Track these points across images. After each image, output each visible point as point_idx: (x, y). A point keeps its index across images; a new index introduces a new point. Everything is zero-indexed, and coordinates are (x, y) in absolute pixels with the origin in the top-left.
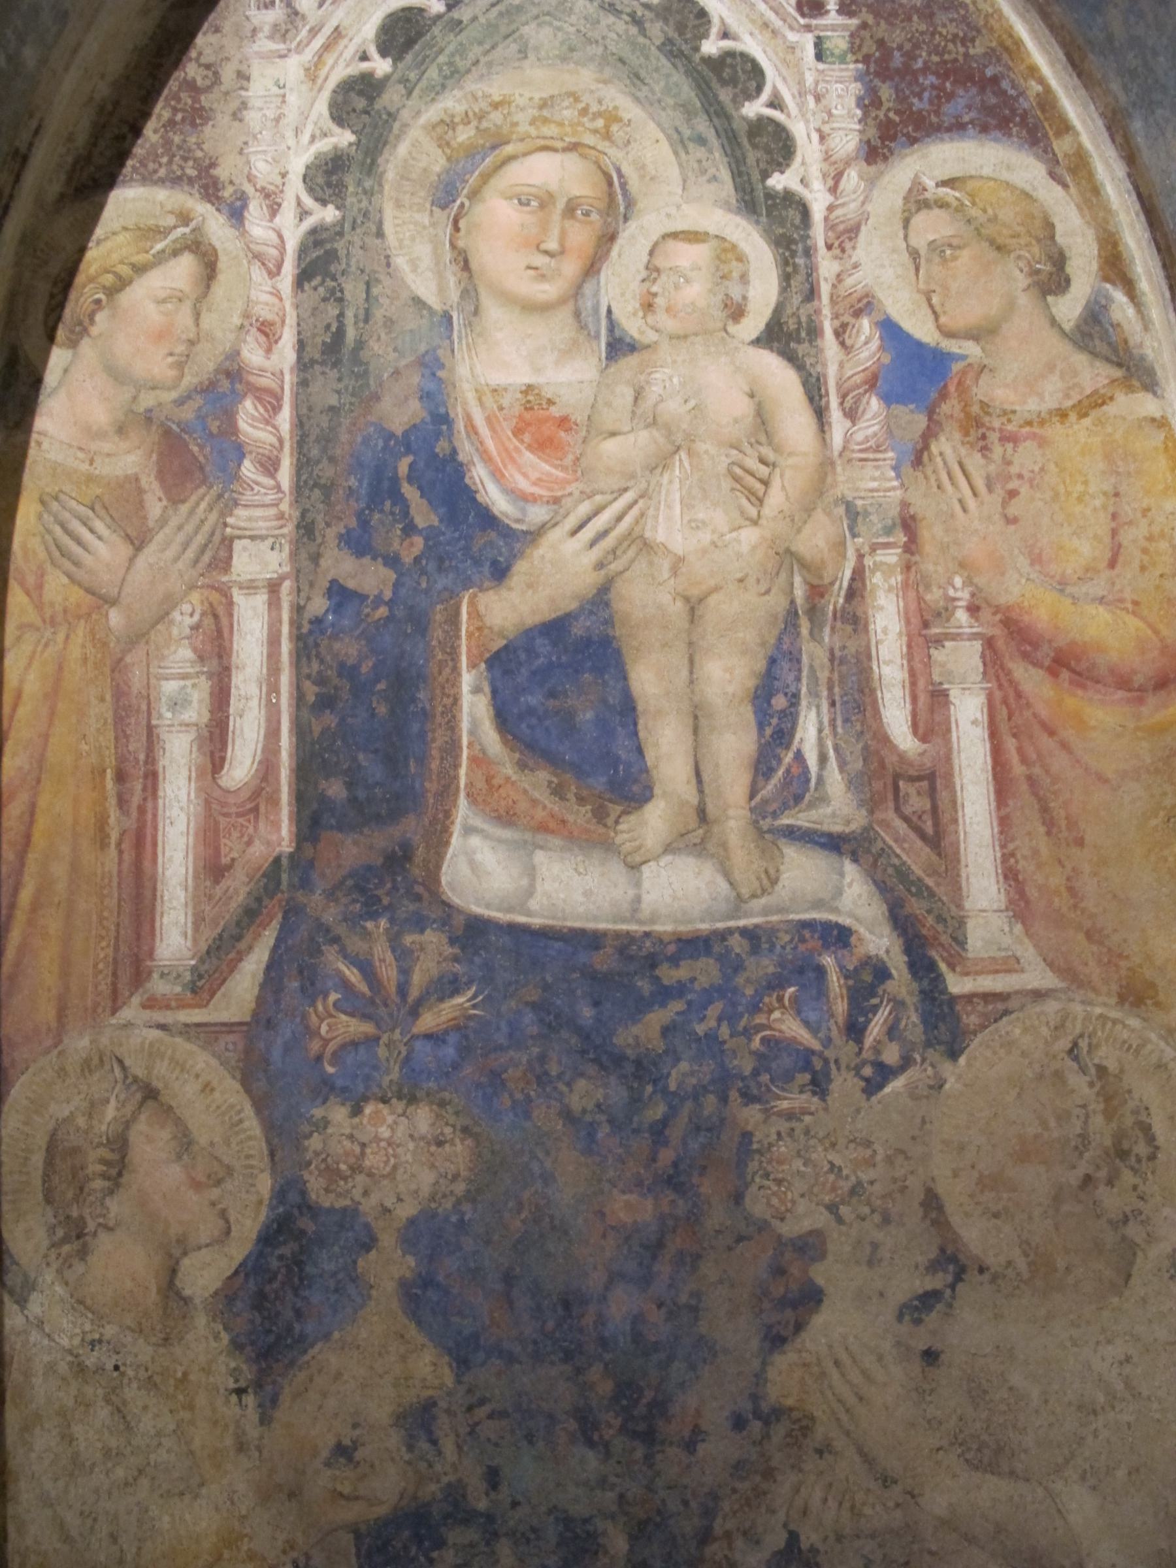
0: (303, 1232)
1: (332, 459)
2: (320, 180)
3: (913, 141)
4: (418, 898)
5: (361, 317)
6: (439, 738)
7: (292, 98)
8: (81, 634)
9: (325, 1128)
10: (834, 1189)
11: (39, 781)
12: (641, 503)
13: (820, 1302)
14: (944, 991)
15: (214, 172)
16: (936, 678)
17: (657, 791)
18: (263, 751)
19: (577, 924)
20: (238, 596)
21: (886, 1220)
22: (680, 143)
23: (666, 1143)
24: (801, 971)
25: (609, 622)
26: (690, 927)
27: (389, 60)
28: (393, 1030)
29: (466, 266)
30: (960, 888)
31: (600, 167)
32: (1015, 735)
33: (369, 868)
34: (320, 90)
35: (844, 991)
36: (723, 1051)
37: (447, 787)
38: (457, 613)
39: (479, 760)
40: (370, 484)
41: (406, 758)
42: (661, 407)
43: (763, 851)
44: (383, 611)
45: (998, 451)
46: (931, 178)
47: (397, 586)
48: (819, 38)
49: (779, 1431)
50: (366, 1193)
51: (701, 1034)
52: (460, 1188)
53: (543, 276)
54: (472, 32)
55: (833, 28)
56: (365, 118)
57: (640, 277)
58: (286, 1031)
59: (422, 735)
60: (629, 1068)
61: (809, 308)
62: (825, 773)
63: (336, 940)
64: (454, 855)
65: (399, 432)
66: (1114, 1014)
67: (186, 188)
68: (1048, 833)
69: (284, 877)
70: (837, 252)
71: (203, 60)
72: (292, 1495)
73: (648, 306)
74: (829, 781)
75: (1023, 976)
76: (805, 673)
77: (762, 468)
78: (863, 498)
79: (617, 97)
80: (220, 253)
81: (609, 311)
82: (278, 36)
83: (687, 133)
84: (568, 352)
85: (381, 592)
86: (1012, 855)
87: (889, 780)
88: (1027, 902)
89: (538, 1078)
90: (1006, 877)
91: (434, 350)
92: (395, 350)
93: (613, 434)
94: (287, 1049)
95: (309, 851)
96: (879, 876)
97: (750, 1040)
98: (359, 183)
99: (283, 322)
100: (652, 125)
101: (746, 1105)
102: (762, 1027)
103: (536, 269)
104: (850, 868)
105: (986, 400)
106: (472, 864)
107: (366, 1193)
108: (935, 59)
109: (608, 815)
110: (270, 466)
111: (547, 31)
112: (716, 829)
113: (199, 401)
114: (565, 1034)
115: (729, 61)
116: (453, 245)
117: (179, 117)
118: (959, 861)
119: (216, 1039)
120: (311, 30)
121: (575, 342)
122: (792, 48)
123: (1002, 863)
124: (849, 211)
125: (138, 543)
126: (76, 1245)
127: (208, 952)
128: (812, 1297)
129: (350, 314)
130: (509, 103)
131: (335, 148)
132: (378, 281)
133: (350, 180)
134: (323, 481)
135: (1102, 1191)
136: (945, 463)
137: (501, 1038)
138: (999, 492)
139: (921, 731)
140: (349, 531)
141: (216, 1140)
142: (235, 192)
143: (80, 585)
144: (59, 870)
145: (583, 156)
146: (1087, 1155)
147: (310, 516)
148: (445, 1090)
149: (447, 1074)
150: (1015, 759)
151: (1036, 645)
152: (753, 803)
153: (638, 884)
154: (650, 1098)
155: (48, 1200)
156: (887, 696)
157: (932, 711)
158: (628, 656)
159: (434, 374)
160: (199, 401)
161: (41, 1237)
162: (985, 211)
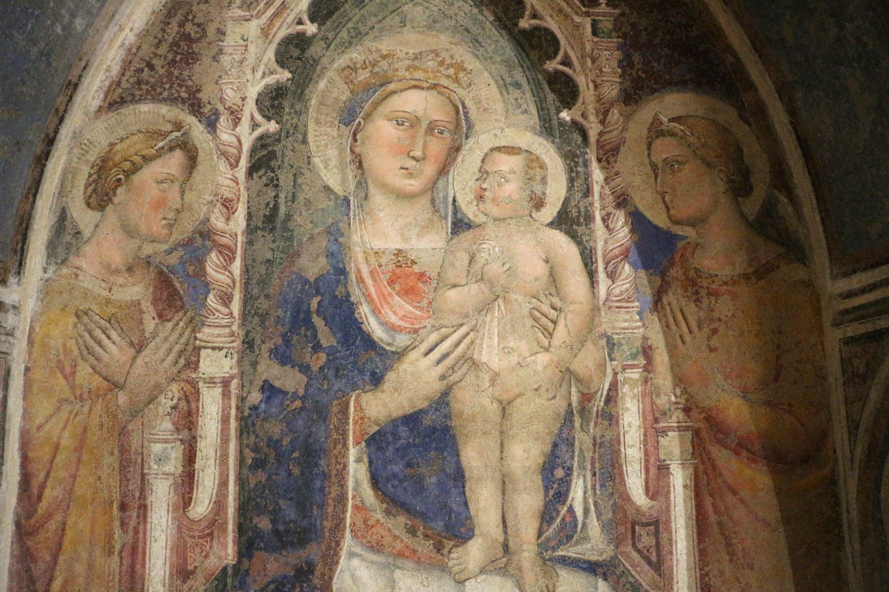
1: (267, 297)
2: (268, 104)
3: (654, 91)
5: (290, 198)
6: (334, 491)
7: (252, 48)
8: (99, 408)
11: (68, 507)
15: (199, 95)
16: (662, 457)
17: (477, 532)
18: (217, 495)
22: (504, 87)
25: (448, 416)
27: (316, 25)
29: (360, 166)
31: (451, 101)
32: (711, 495)
33: (285, 577)
34: (270, 43)
37: (337, 526)
38: (347, 407)
40: (292, 314)
41: (311, 505)
44: (298, 404)
45: (705, 301)
46: (665, 116)
47: (307, 386)
48: (594, 20)
53: (411, 174)
56: (299, 63)
57: (475, 178)
59: (322, 489)
62: (588, 521)
64: (341, 571)
65: (312, 280)
67: (180, 105)
68: (731, 560)
69: (229, 581)
70: (605, 164)
71: (196, 21)
73: (481, 198)
74: (590, 526)
76: (576, 454)
77: (553, 311)
78: (617, 333)
79: (463, 54)
80: (200, 151)
81: (454, 200)
82: (245, 6)
83: (509, 80)
84: (426, 228)
85: (297, 391)
86: (707, 575)
87: (629, 526)
91: (337, 223)
92: (311, 222)
93: (455, 286)
95: (246, 563)
98: (292, 106)
99: (239, 200)
100: (486, 74)
103: (407, 169)
104: (601, 584)
105: (698, 267)
106: (353, 576)
108: (668, 37)
110: (226, 299)
111: (420, 9)
112: (515, 558)
115: (537, 33)
116: (352, 151)
117: (178, 58)
118: (672, 579)
122: (577, 26)
124: (613, 136)
125: (139, 347)
129: (282, 196)
130: (394, 55)
131: (278, 82)
132: (302, 174)
133: (286, 104)
134: (260, 311)
138: (706, 330)
139: (650, 494)
143: (100, 374)
144: (80, 568)
150: (710, 510)
151: (726, 435)
152: (540, 541)
156: (630, 469)
159: (336, 240)
160: (180, 252)
162: (699, 140)
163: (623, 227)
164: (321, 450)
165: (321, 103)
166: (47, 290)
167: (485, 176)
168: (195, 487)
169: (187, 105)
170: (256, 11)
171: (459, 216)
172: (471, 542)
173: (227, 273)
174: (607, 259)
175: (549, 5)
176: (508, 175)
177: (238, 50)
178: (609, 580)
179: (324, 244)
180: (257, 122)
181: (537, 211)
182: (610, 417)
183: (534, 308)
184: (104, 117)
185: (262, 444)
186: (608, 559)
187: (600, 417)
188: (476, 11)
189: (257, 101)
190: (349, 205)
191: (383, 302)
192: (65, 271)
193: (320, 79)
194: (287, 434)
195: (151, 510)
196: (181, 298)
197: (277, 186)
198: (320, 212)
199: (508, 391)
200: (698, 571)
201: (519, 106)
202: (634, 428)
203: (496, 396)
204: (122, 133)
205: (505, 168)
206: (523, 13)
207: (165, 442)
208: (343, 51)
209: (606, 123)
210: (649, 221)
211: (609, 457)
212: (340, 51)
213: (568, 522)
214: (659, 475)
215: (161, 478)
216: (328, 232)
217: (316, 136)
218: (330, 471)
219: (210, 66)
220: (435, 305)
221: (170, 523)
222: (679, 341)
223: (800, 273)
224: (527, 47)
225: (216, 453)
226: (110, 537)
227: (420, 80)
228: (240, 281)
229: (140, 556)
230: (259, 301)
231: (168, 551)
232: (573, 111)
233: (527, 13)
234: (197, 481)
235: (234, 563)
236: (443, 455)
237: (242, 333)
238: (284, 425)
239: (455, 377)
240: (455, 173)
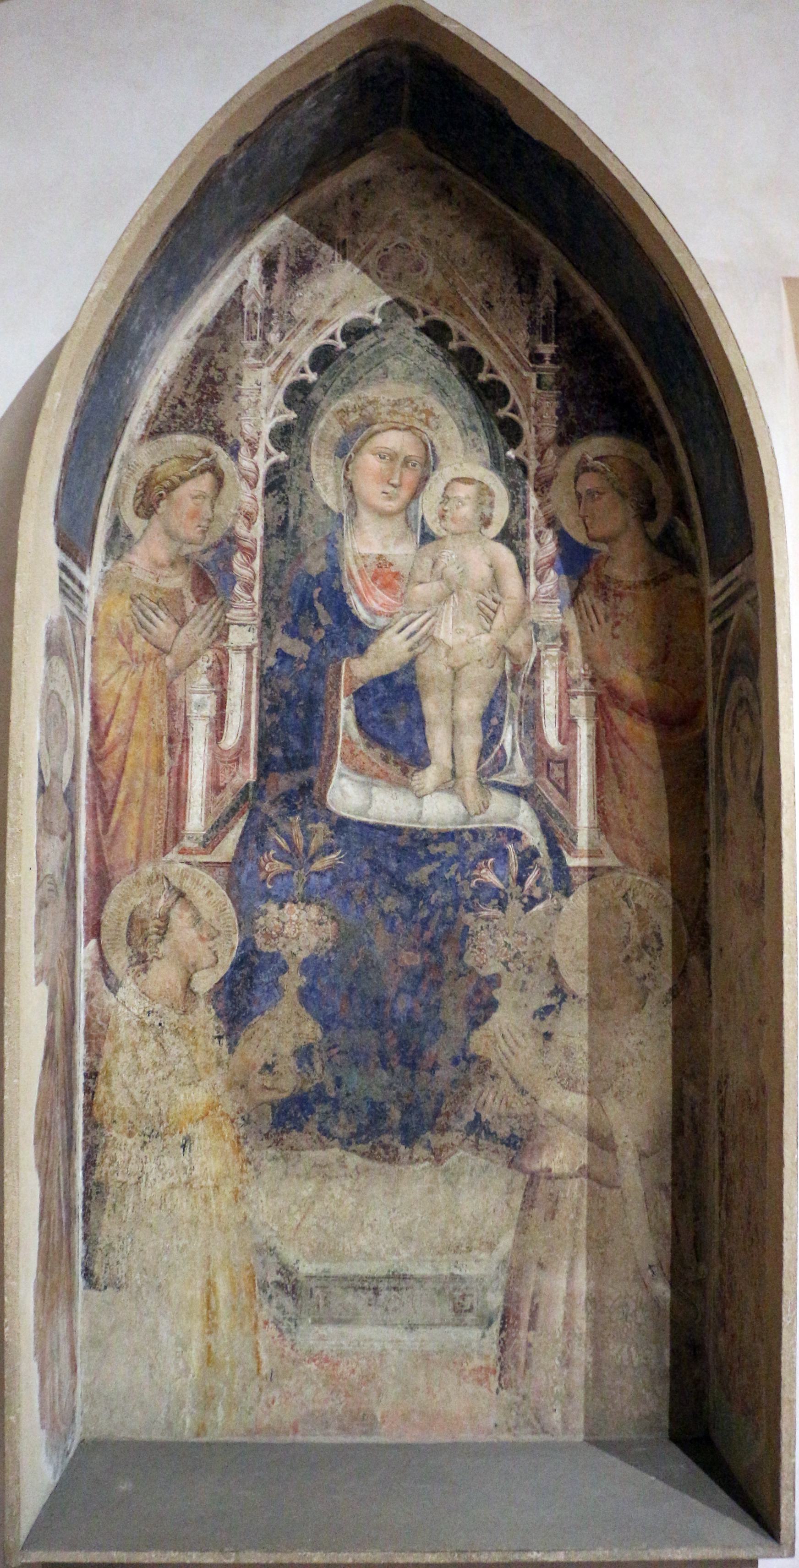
0: (253, 964)
1: (280, 587)
2: (278, 438)
3: (583, 435)
4: (315, 807)
6: (329, 730)
7: (265, 392)
10: (506, 955)
12: (433, 619)
13: (496, 1007)
15: (223, 429)
16: (572, 713)
20: (232, 654)
21: (530, 970)
23: (428, 929)
25: (414, 678)
29: (351, 489)
32: (608, 744)
33: (292, 791)
38: (340, 670)
39: (348, 741)
45: (612, 600)
47: (311, 653)
49: (474, 1067)
50: (284, 946)
52: (329, 945)
55: (548, 370)
56: (302, 405)
58: (249, 866)
59: (320, 728)
61: (524, 521)
63: (275, 825)
65: (314, 574)
66: (646, 880)
69: (251, 794)
70: (540, 493)
72: (242, 1087)
73: (442, 517)
76: (508, 708)
79: (433, 402)
81: (423, 518)
84: (400, 539)
93: (421, 583)
94: (250, 876)
95: (263, 781)
98: (298, 441)
100: (450, 419)
102: (477, 877)
104: (523, 803)
107: (284, 946)
110: (249, 589)
111: (399, 363)
112: (460, 781)
114: (382, 875)
116: (345, 478)
117: (205, 397)
122: (525, 380)
124: (547, 471)
125: (182, 623)
126: (143, 966)
128: (492, 1005)
133: (293, 439)
135: (635, 965)
137: (352, 875)
144: (139, 785)
145: (414, 434)
146: (628, 946)
150: (607, 755)
153: (421, 805)
155: (129, 943)
156: (547, 721)
157: (568, 729)
161: (125, 960)
165: (321, 439)
166: (106, 580)
172: (428, 769)
179: (324, 548)
182: (534, 682)
184: (146, 444)
188: (444, 365)
192: (120, 565)
196: (214, 587)
197: (287, 504)
204: (162, 458)
216: (326, 540)
220: (406, 596)
223: (690, 581)
224: (484, 398)
226: (160, 762)
229: (184, 776)
232: (518, 449)
237: (261, 614)
239: (419, 650)
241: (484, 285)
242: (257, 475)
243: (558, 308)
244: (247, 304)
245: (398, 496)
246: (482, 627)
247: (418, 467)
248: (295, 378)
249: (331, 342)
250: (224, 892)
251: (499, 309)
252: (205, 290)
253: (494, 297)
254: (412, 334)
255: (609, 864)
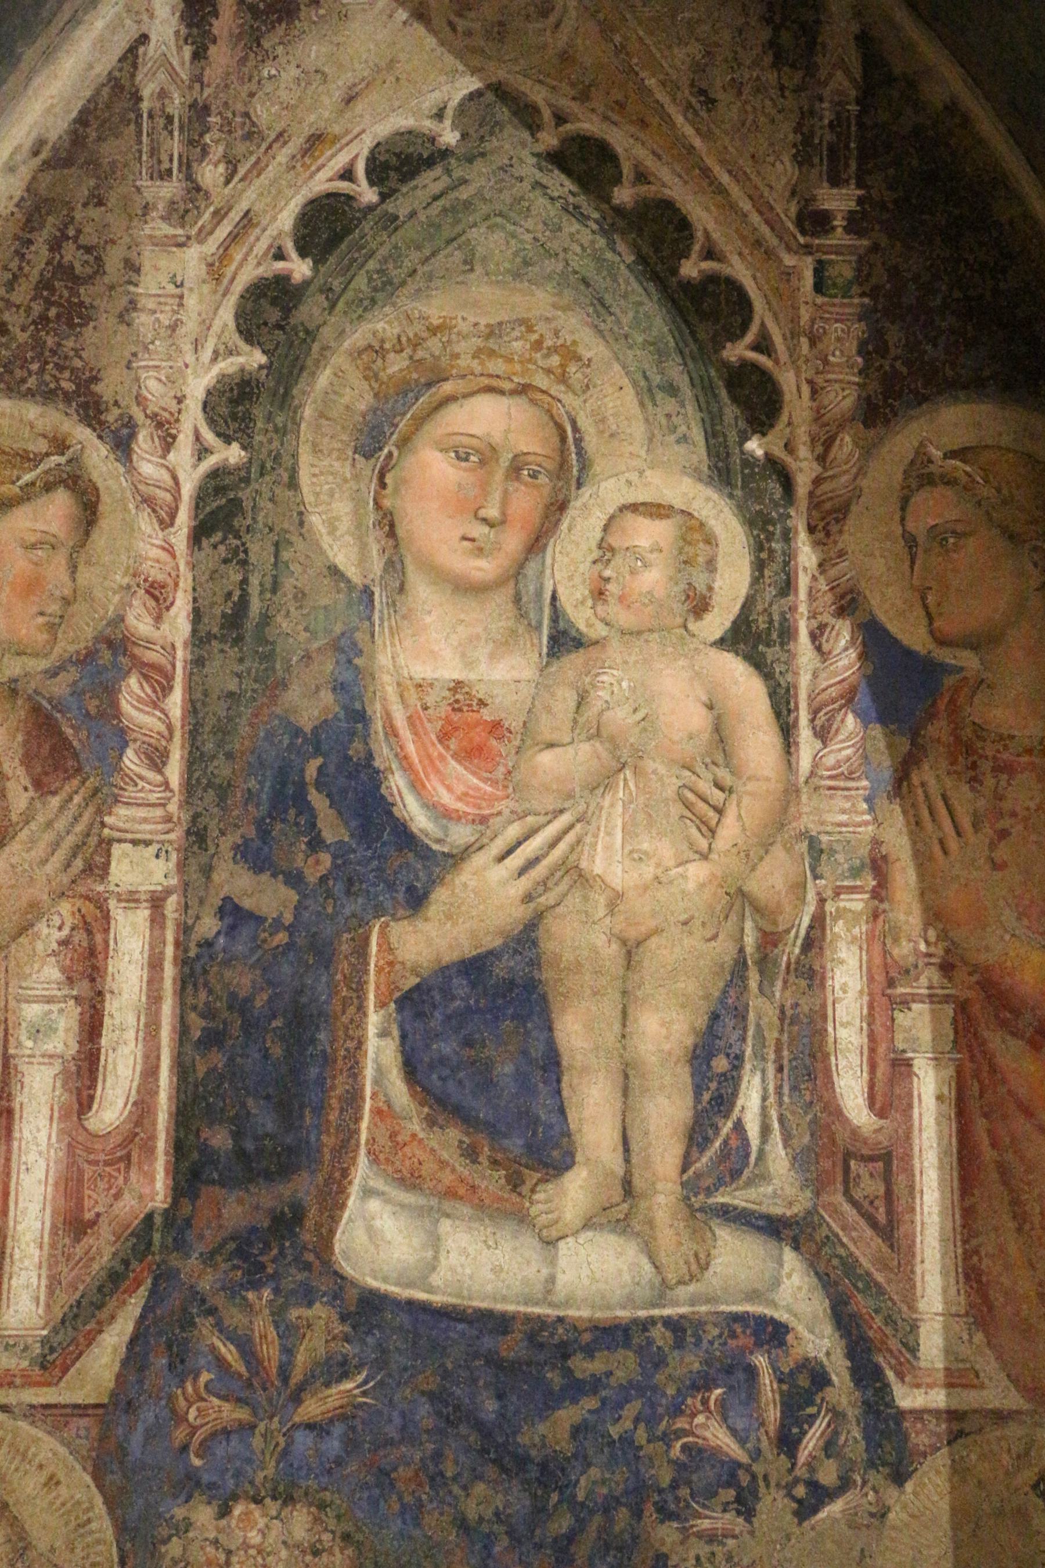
1: (229, 756)
2: (224, 410)
3: (922, 399)
4: (308, 1267)
5: (268, 586)
6: (341, 1085)
7: (191, 301)
9: (187, 1531)
12: (578, 826)
14: (891, 1404)
15: (98, 388)
16: (900, 1046)
17: (579, 1158)
18: (138, 1092)
19: (484, 1305)
22: (647, 393)
24: (729, 1370)
25: (535, 963)
26: (607, 1314)
27: (309, 261)
28: (271, 1418)
29: (392, 533)
30: (914, 1287)
31: (552, 417)
32: (986, 1116)
33: (254, 1230)
34: (224, 295)
35: (777, 1397)
36: (638, 1458)
38: (366, 940)
40: (273, 787)
41: (302, 1107)
42: (608, 714)
43: (695, 1231)
44: (282, 937)
45: (990, 782)
46: (937, 448)
47: (299, 908)
48: (820, 262)
51: (616, 1437)
53: (480, 550)
54: (409, 231)
55: (838, 250)
57: (590, 559)
58: (148, 1415)
59: (321, 1081)
60: (534, 1472)
62: (768, 1148)
63: (212, 1311)
64: (350, 1220)
65: (308, 729)
68: (1019, 1230)
69: (157, 1237)
70: (821, 535)
71: (82, 240)
73: (599, 594)
74: (771, 1157)
75: (985, 1393)
76: (750, 1033)
77: (717, 793)
78: (827, 833)
81: (554, 598)
83: (657, 379)
84: (504, 644)
86: (976, 1252)
88: (990, 1309)
89: (432, 1479)
90: (967, 1276)
92: (306, 629)
93: (551, 745)
94: (149, 1436)
95: (186, 1209)
96: (821, 1268)
97: (669, 1446)
98: (269, 418)
99: (176, 585)
100: (617, 367)
101: (662, 1522)
102: (686, 1433)
103: (473, 540)
104: (789, 1256)
108: (957, 294)
109: (523, 1182)
110: (157, 759)
111: (498, 236)
112: (643, 1204)
113: (72, 674)
114: (463, 1429)
115: (711, 288)
116: (378, 506)
117: (53, 312)
118: (914, 1256)
119: (66, 1424)
120: (216, 213)
121: (513, 632)
122: (788, 274)
123: (964, 1260)
127: (63, 1322)
129: (255, 581)
130: (451, 328)
131: (242, 370)
132: (290, 543)
133: (258, 412)
134: (218, 781)
136: (927, 796)
137: (392, 1431)
139: (878, 1106)
140: (246, 842)
141: (57, 1544)
142: (121, 415)
147: (202, 821)
148: (326, 1489)
149: (329, 1472)
151: (1017, 1013)
152: (685, 1177)
153: (553, 1262)
154: (555, 1506)
156: (842, 1063)
157: (891, 1082)
158: (555, 1004)
159: (350, 662)
162: (999, 490)
163: (846, 649)
164: (319, 1015)
167: (608, 555)
168: (101, 1077)
169: (74, 404)
170: (196, 229)
171: (562, 625)
172: (569, 1176)
173: (158, 713)
174: (816, 704)
175: (737, 231)
176: (649, 555)
177: (166, 304)
178: (803, 1249)
179: (330, 667)
180: (206, 444)
181: (696, 620)
183: (684, 786)
185: (218, 1004)
186: (801, 1215)
187: (792, 973)
188: (601, 242)
189: (205, 405)
190: (372, 601)
191: (429, 770)
193: (318, 367)
194: (262, 989)
195: (21, 1117)
196: (76, 756)
197: (244, 563)
198: (322, 611)
199: (637, 924)
200: (959, 1244)
201: (673, 429)
202: (852, 995)
203: (615, 931)
205: (643, 542)
206: (689, 248)
207: (48, 1002)
208: (360, 316)
209: (829, 460)
210: (895, 639)
211: (805, 1040)
212: (355, 316)
213: (734, 1146)
214: (893, 1074)
215: (40, 1064)
216: (336, 646)
217: (314, 475)
218: (335, 1051)
219: (115, 332)
220: (517, 776)
221: (54, 1139)
222: (937, 849)
224: (693, 319)
225: (139, 1020)
227: (498, 376)
228: (183, 727)
230: (216, 763)
231: (50, 1189)
232: (769, 437)
233: (697, 247)
234: (105, 1067)
235: (166, 1206)
236: (525, 1027)
237: (186, 817)
238: (258, 972)
239: (547, 899)
240: (558, 550)
241: (695, 49)
242: (177, 498)
243: (866, 97)
244: (147, 91)
245: (497, 547)
246: (691, 845)
247: (543, 479)
248: (260, 271)
249: (343, 186)
250: (88, 1479)
251: (729, 110)
252: (49, 55)
253: (718, 79)
254: (528, 168)
255: (995, 1404)
